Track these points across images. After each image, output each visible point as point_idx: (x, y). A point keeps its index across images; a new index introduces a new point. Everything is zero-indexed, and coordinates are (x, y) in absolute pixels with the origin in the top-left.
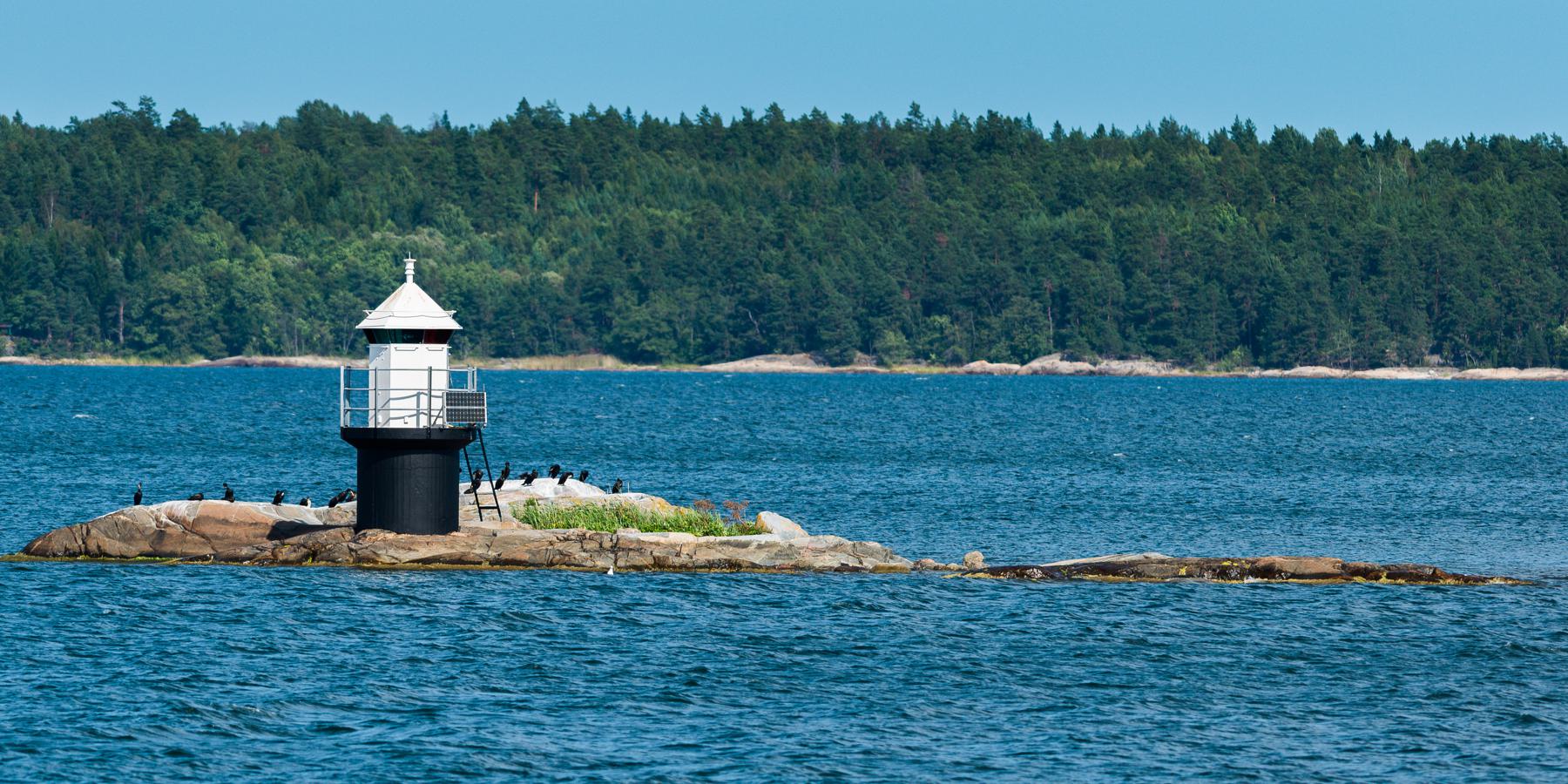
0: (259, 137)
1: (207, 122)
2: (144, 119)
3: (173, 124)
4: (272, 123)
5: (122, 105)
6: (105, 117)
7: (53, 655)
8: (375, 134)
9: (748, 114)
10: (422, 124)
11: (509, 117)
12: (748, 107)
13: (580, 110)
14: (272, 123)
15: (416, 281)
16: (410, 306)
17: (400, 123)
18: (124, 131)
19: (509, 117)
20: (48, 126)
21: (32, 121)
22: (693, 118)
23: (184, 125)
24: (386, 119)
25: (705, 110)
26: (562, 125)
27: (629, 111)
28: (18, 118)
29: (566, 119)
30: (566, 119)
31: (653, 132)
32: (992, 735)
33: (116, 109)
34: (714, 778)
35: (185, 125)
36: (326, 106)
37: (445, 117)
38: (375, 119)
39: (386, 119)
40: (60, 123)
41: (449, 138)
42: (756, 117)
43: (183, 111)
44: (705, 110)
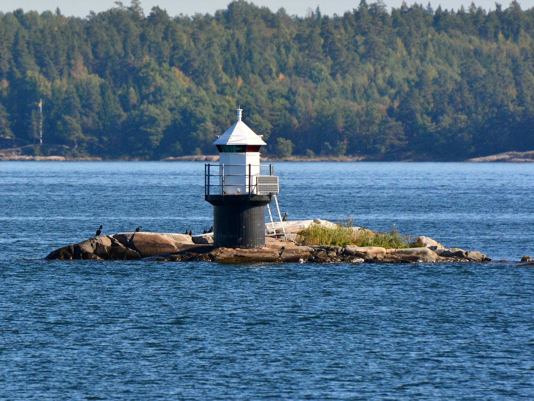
0: (201, 23)
1: (172, 14)
2: (134, 13)
3: (152, 15)
4: (212, 14)
5: (121, 4)
6: (111, 11)
7: (527, 348)
8: (271, 20)
9: (498, 6)
10: (303, 14)
11: (354, 10)
12: (499, 2)
13: (398, 6)
14: (212, 14)
15: (243, 120)
16: (242, 134)
17: (290, 12)
18: (113, 18)
19: (354, 10)
20: (76, 16)
21: (66, 13)
22: (467, 10)
23: (158, 14)
24: (282, 11)
25: (473, 4)
26: (386, 14)
27: (429, 5)
28: (58, 11)
29: (389, 11)
30: (389, 11)
31: (440, 20)
32: (28, 344)
33: (117, 6)
34: (372, 398)
35: (158, 15)
36: (78, 20)
37: (318, 9)
38: (274, 10)
39: (282, 10)
40: (83, 14)
41: (318, 23)
42: (503, 9)
43: (158, 8)
44: (473, 4)
